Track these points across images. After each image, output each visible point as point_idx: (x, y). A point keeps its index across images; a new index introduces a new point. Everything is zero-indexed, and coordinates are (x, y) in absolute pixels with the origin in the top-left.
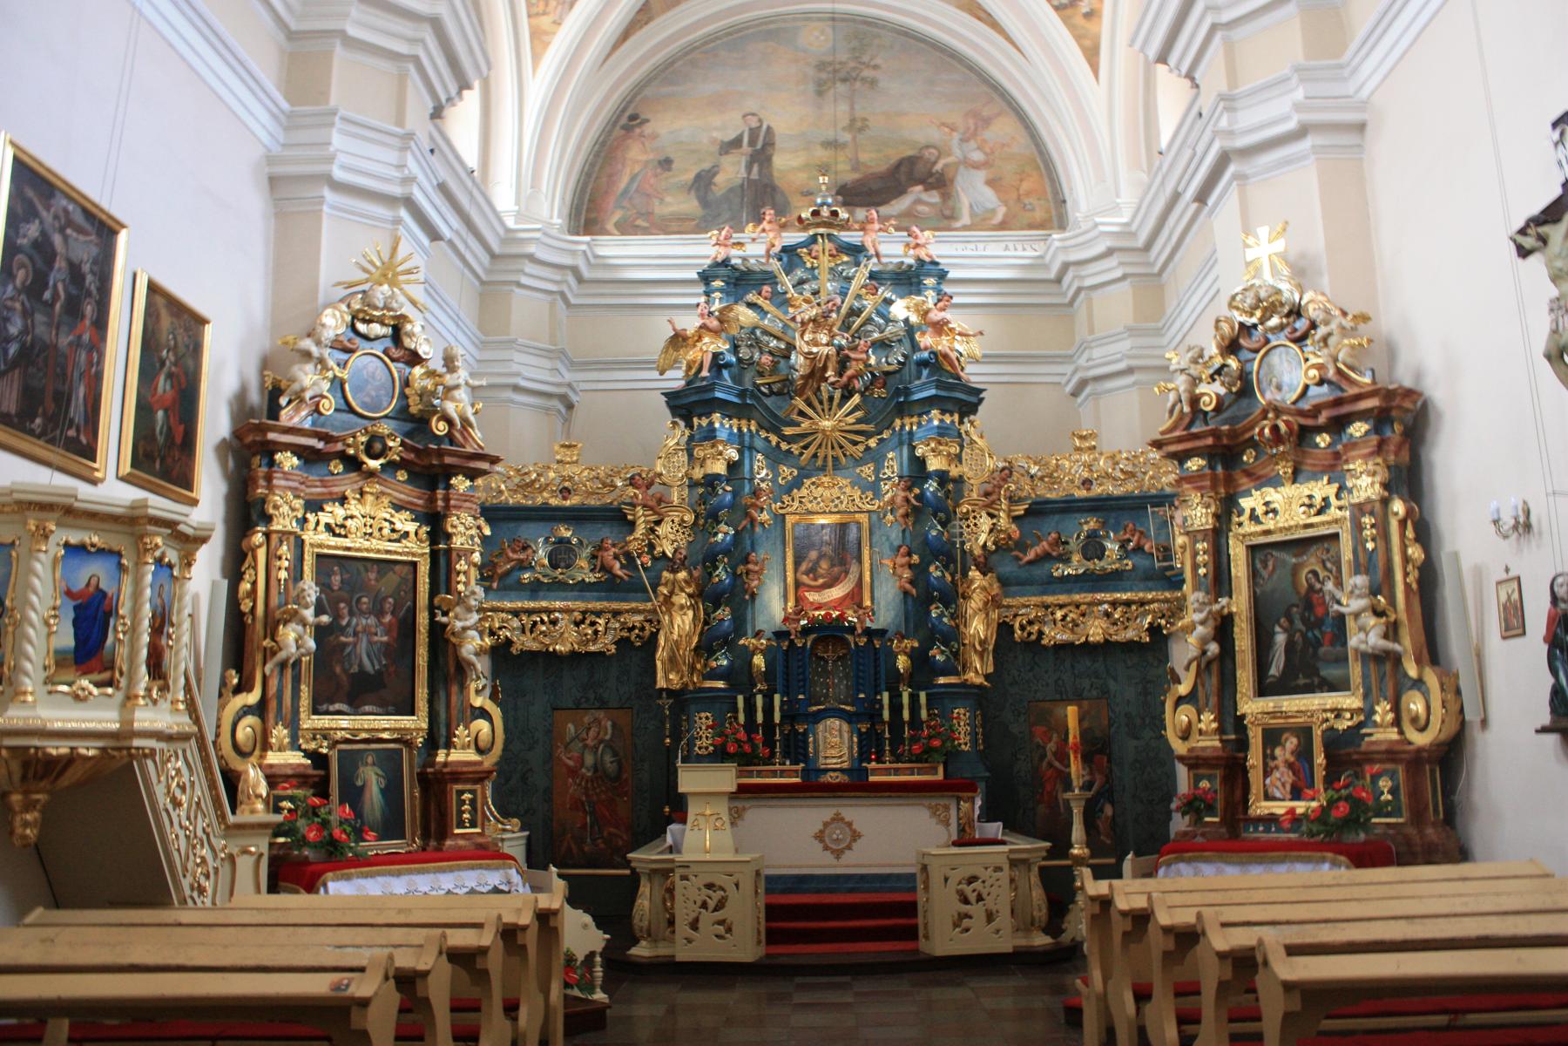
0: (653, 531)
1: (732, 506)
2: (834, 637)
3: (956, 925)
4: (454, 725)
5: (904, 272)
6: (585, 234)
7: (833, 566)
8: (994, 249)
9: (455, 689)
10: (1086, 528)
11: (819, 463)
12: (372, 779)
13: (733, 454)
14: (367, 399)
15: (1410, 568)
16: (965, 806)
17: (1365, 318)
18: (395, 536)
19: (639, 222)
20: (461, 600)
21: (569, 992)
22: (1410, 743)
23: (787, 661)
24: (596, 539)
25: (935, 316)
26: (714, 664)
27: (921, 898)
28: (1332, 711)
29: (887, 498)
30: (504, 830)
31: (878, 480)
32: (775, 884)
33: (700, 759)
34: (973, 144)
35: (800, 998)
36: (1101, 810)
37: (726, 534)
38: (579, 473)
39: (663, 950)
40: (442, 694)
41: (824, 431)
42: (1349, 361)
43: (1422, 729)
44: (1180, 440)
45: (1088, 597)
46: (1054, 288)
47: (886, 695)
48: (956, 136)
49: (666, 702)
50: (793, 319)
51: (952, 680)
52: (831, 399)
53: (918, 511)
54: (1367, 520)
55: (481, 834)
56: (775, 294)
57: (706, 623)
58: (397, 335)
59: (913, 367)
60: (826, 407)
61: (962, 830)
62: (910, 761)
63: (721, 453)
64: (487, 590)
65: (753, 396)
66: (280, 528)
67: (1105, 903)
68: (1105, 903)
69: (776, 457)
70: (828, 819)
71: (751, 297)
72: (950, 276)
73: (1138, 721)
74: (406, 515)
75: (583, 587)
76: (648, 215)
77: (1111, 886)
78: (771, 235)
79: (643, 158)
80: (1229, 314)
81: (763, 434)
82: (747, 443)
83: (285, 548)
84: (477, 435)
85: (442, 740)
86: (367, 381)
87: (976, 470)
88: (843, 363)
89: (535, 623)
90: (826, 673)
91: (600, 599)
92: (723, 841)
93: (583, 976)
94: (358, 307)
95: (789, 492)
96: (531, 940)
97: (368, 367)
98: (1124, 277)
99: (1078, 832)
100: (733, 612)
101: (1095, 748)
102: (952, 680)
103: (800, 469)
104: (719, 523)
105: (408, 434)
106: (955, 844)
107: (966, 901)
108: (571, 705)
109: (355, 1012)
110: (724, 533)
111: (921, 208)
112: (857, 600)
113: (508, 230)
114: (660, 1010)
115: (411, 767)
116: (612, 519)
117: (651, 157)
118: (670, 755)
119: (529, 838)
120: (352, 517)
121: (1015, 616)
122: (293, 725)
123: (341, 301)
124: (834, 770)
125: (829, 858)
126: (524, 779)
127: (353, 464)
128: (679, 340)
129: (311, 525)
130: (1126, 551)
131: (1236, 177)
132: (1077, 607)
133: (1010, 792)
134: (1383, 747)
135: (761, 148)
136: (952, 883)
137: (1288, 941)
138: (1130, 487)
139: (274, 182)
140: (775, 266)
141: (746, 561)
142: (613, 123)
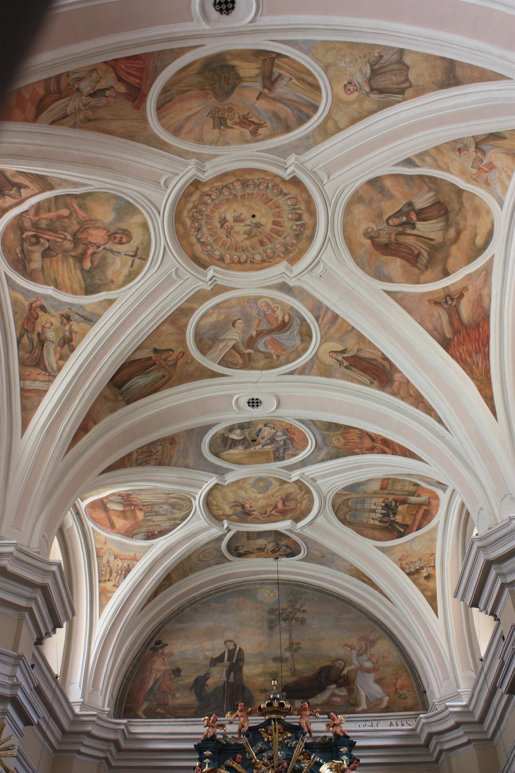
5: (327, 743)
34: (365, 657)
56: (244, 759)
78: (242, 719)
79: (163, 668)
98: (469, 742)
111: (335, 699)
113: (75, 715)
117: (168, 668)
135: (235, 661)
140: (244, 740)
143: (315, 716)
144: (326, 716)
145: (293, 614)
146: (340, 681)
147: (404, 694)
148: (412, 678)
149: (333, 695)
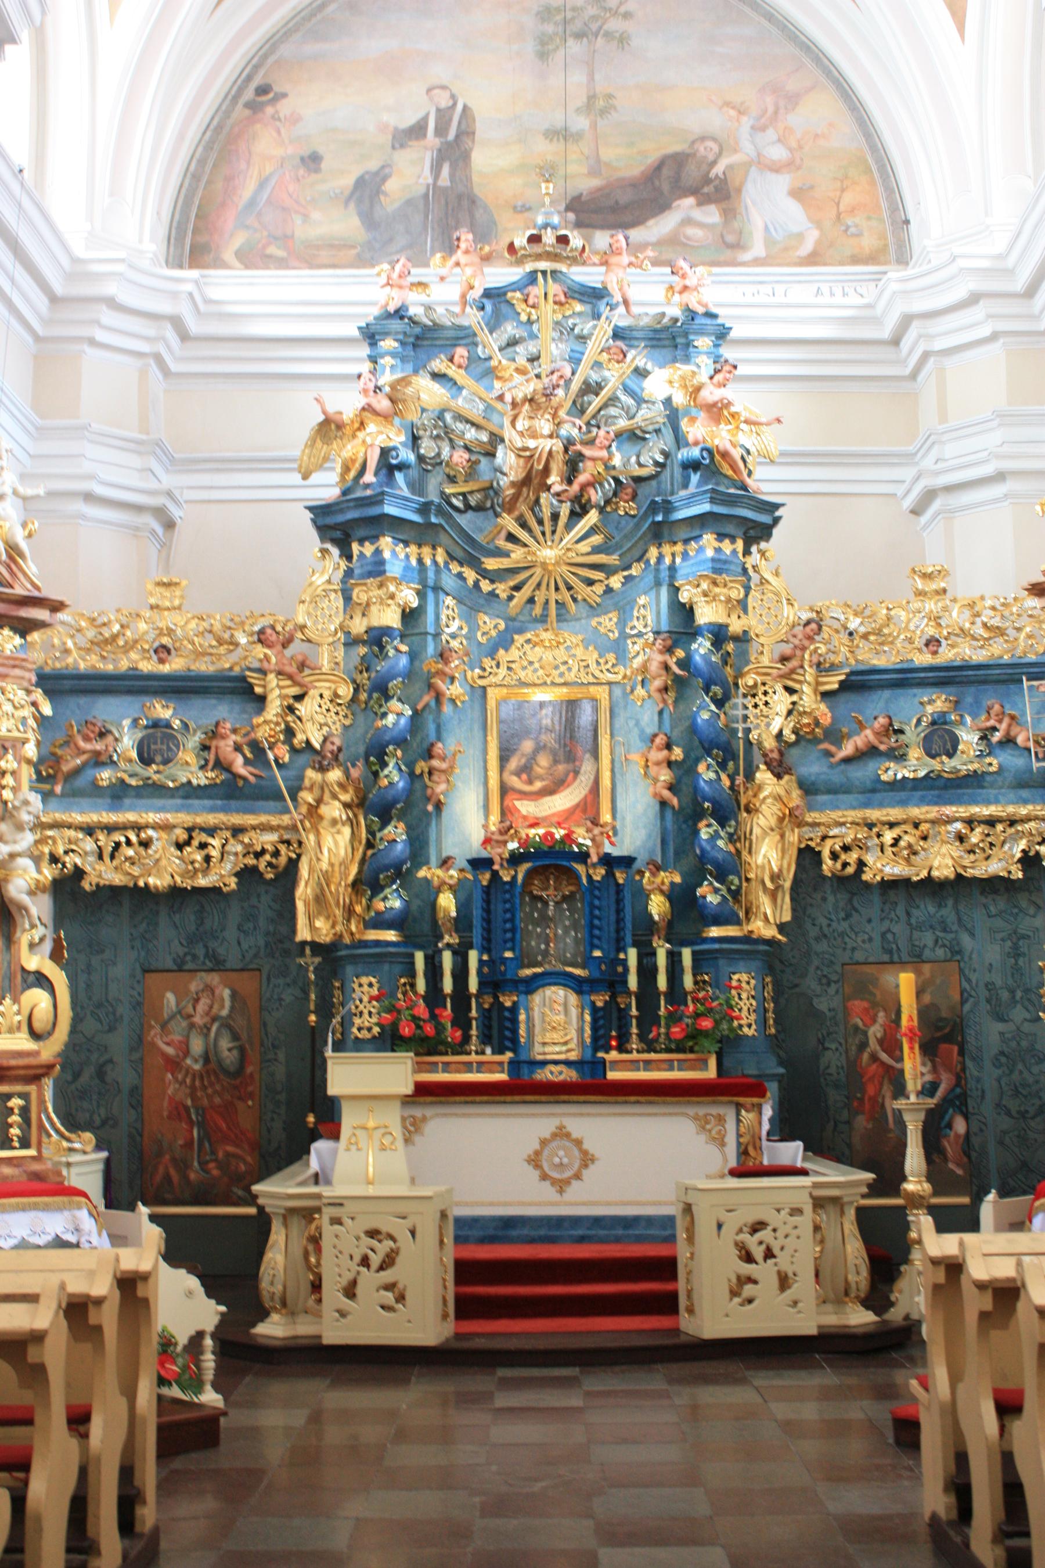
0: (291, 709)
1: (410, 675)
2: (557, 867)
3: (734, 1293)
5: (666, 329)
6: (191, 267)
7: (556, 762)
10: (930, 709)
11: (538, 610)
13: (409, 597)
16: (747, 1117)
19: (272, 250)
21: (165, 1391)
23: (487, 901)
24: (209, 722)
25: (711, 394)
26: (381, 906)
27: (682, 1252)
29: (637, 663)
30: (71, 1150)
31: (624, 636)
32: (467, 1229)
33: (359, 1045)
34: (771, 134)
35: (503, 1400)
36: (950, 1126)
37: (399, 714)
38: (182, 624)
39: (304, 1328)
41: (544, 565)
45: (932, 812)
46: (888, 353)
47: (632, 955)
48: (746, 122)
49: (311, 962)
50: (501, 398)
51: (731, 931)
52: (555, 517)
53: (680, 684)
55: (38, 1158)
56: (473, 360)
57: (370, 845)
59: (678, 471)
60: (548, 528)
61: (743, 1152)
62: (669, 1050)
63: (392, 597)
64: (46, 796)
65: (440, 512)
67: (953, 1268)
68: (954, 1268)
69: (474, 602)
70: (547, 1135)
71: (439, 364)
72: (733, 334)
73: (1005, 995)
75: (189, 792)
76: (286, 239)
77: (961, 1244)
78: (469, 271)
79: (278, 152)
81: (455, 568)
82: (431, 582)
84: (31, 568)
87: (767, 625)
88: (573, 465)
89: (118, 845)
90: (544, 920)
91: (213, 810)
92: (398, 1171)
93: (186, 1368)
95: (492, 654)
96: (108, 1318)
98: (994, 337)
99: (914, 1159)
100: (410, 829)
101: (941, 1035)
102: (731, 931)
103: (509, 619)
104: (388, 698)
106: (735, 1173)
107: (749, 1258)
108: (170, 964)
110: (396, 715)
111: (691, 231)
112: (590, 814)
113: (75, 260)
114: (299, 1418)
116: (233, 692)
117: (290, 150)
118: (315, 1040)
119: (108, 1162)
121: (824, 838)
124: (556, 1062)
125: (548, 1191)
126: (101, 1074)
128: (330, 428)
130: (989, 744)
132: (916, 826)
133: (817, 1101)
135: (453, 139)
136: (729, 1230)
138: (997, 651)
140: (473, 318)
141: (429, 755)
142: (233, 97)
143: (640, 267)
144: (668, 270)
145: (599, 23)
146: (706, 190)
147: (856, 226)
148: (880, 189)
149: (688, 221)
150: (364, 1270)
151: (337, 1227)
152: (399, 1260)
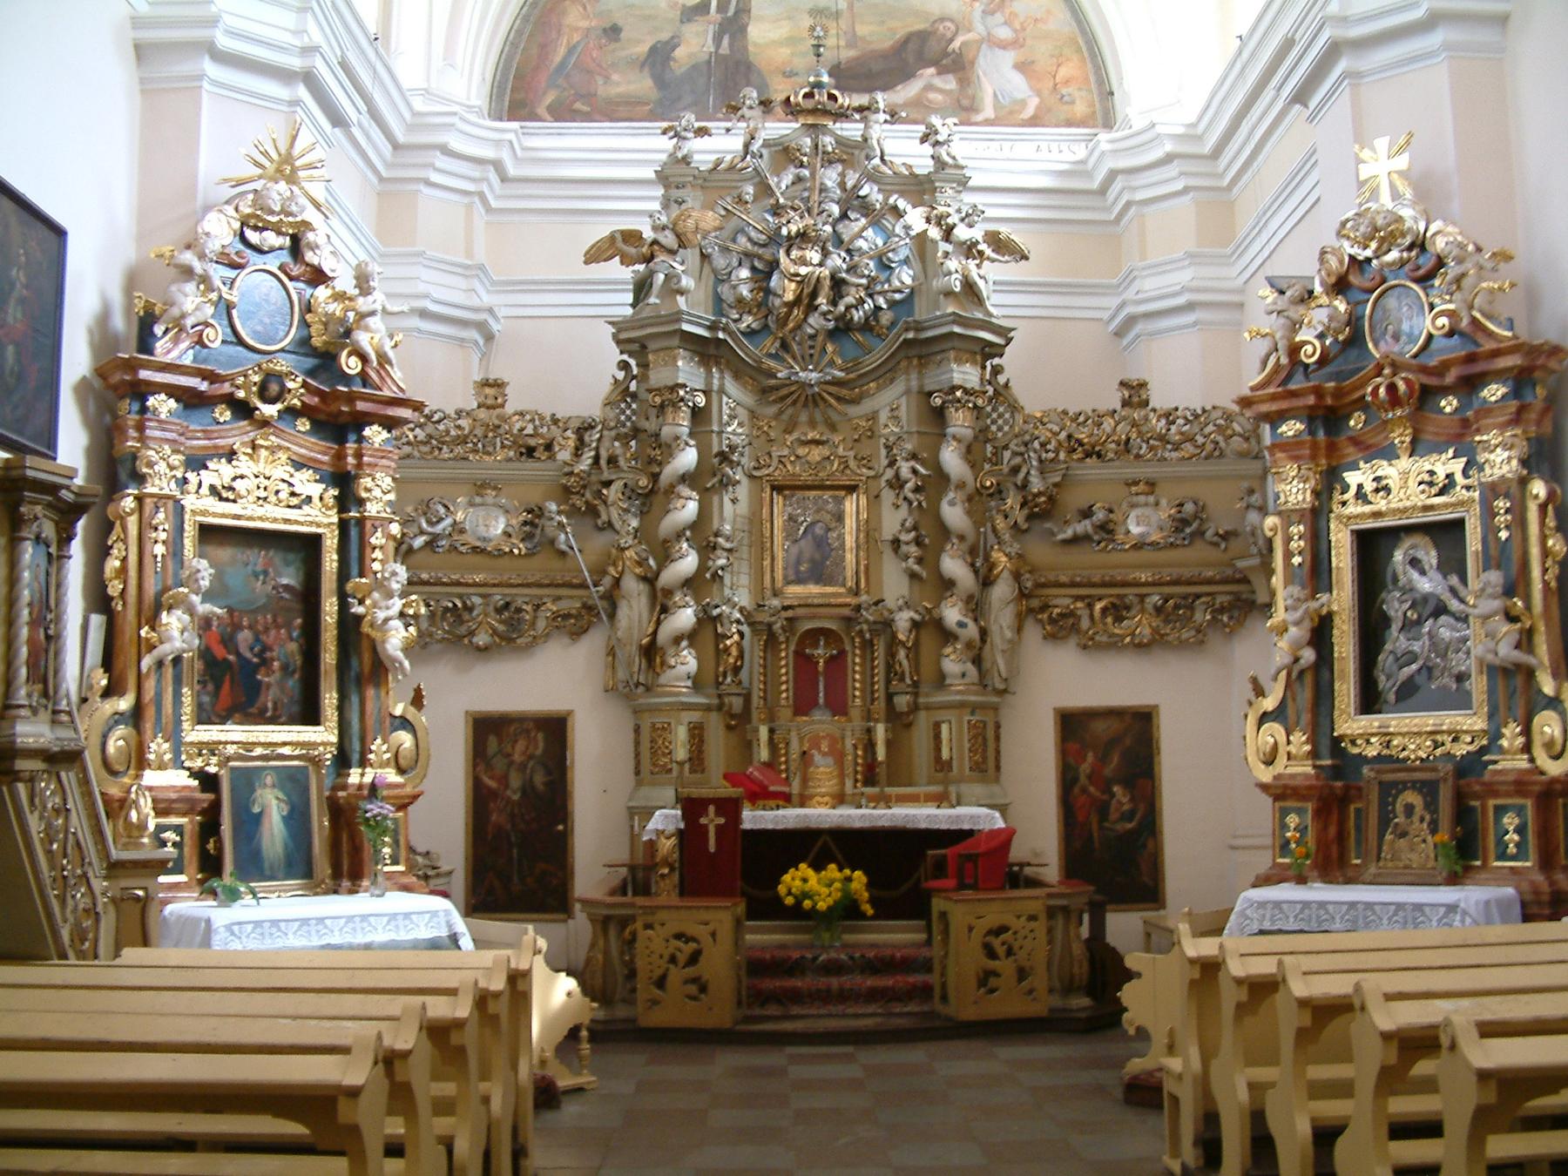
4: (369, 738)
8: (1025, 149)
9: (370, 693)
12: (272, 805)
14: (259, 328)
15: (1549, 563)
17: (1504, 257)
18: (295, 501)
19: (578, 106)
20: (380, 585)
22: (1542, 773)
28: (1449, 732)
34: (999, 17)
40: (355, 699)
42: (1486, 308)
43: (1557, 757)
44: (1274, 398)
54: (1501, 504)
58: (296, 247)
66: (155, 490)
68: (1210, 968)
74: (307, 474)
76: (589, 97)
79: (584, 24)
80: (1337, 245)
83: (161, 516)
84: (397, 374)
85: (356, 757)
86: (258, 305)
94: (249, 211)
97: (260, 291)
105: (311, 373)
107: (991, 954)
109: (343, 1104)
111: (932, 96)
113: (415, 114)
115: (320, 789)
120: (242, 477)
122: (175, 737)
123: (227, 202)
127: (243, 410)
129: (192, 487)
131: (1345, 75)
134: (1511, 778)
137: (1480, 1018)
139: (142, 52)
148: (1090, 66)
149: (929, 87)
150: (671, 966)
151: (650, 932)
152: (702, 959)
